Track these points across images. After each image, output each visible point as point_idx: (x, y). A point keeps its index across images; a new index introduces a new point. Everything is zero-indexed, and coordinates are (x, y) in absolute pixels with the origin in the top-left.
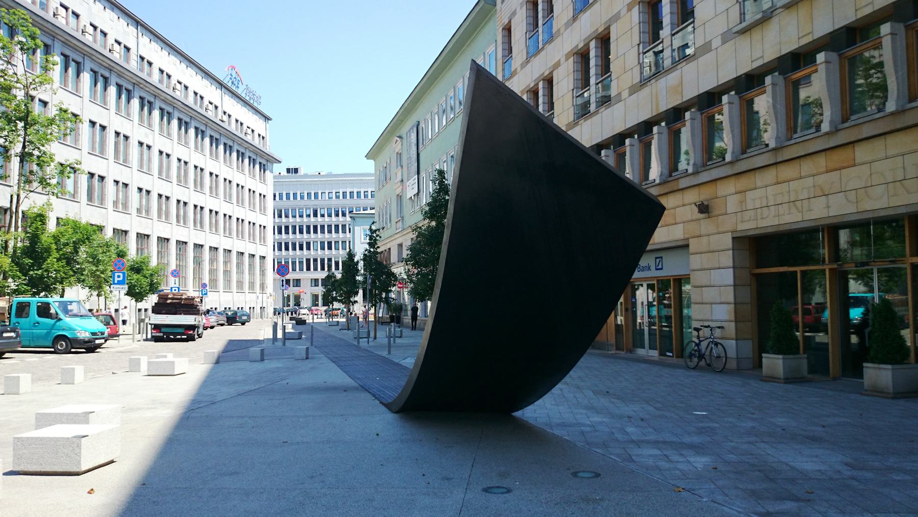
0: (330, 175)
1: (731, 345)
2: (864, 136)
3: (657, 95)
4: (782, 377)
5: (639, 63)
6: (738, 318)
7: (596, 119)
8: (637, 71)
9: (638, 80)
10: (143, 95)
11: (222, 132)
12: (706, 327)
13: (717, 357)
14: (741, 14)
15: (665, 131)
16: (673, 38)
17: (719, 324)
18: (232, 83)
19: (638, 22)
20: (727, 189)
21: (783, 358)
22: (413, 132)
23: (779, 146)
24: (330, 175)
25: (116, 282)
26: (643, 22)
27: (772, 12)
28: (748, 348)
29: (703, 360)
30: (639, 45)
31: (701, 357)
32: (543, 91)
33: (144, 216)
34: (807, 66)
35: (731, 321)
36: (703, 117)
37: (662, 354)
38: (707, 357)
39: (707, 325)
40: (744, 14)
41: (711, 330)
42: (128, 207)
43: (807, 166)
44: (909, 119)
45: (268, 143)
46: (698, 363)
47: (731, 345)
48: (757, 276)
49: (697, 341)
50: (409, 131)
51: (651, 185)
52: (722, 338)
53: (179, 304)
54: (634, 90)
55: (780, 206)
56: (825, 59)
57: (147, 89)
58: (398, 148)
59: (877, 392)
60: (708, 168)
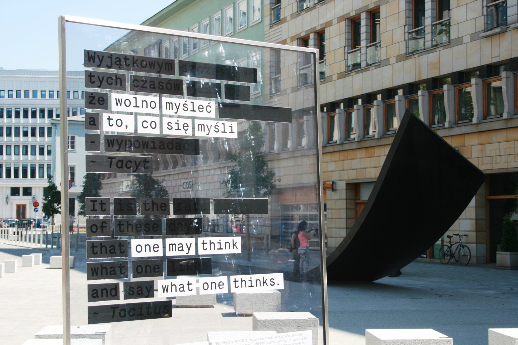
1: (472, 247)
3: (419, 66)
4: (509, 266)
5: (345, 59)
6: (478, 230)
8: (343, 63)
9: (404, 52)
12: (456, 235)
13: (464, 255)
14: (406, 48)
15: (403, 99)
16: (367, 49)
17: (464, 233)
19: (404, 9)
21: (510, 254)
23: (509, 118)
26: (348, 32)
27: (506, 28)
28: (483, 249)
29: (454, 258)
30: (405, 26)
31: (452, 255)
34: (467, 82)
35: (473, 231)
36: (456, 89)
38: (456, 256)
39: (457, 234)
40: (408, 47)
41: (460, 237)
44: (514, 123)
46: (450, 260)
47: (472, 247)
48: (491, 201)
49: (449, 245)
51: (351, 141)
52: (466, 243)
55: (508, 156)
56: (422, 94)
60: (459, 125)
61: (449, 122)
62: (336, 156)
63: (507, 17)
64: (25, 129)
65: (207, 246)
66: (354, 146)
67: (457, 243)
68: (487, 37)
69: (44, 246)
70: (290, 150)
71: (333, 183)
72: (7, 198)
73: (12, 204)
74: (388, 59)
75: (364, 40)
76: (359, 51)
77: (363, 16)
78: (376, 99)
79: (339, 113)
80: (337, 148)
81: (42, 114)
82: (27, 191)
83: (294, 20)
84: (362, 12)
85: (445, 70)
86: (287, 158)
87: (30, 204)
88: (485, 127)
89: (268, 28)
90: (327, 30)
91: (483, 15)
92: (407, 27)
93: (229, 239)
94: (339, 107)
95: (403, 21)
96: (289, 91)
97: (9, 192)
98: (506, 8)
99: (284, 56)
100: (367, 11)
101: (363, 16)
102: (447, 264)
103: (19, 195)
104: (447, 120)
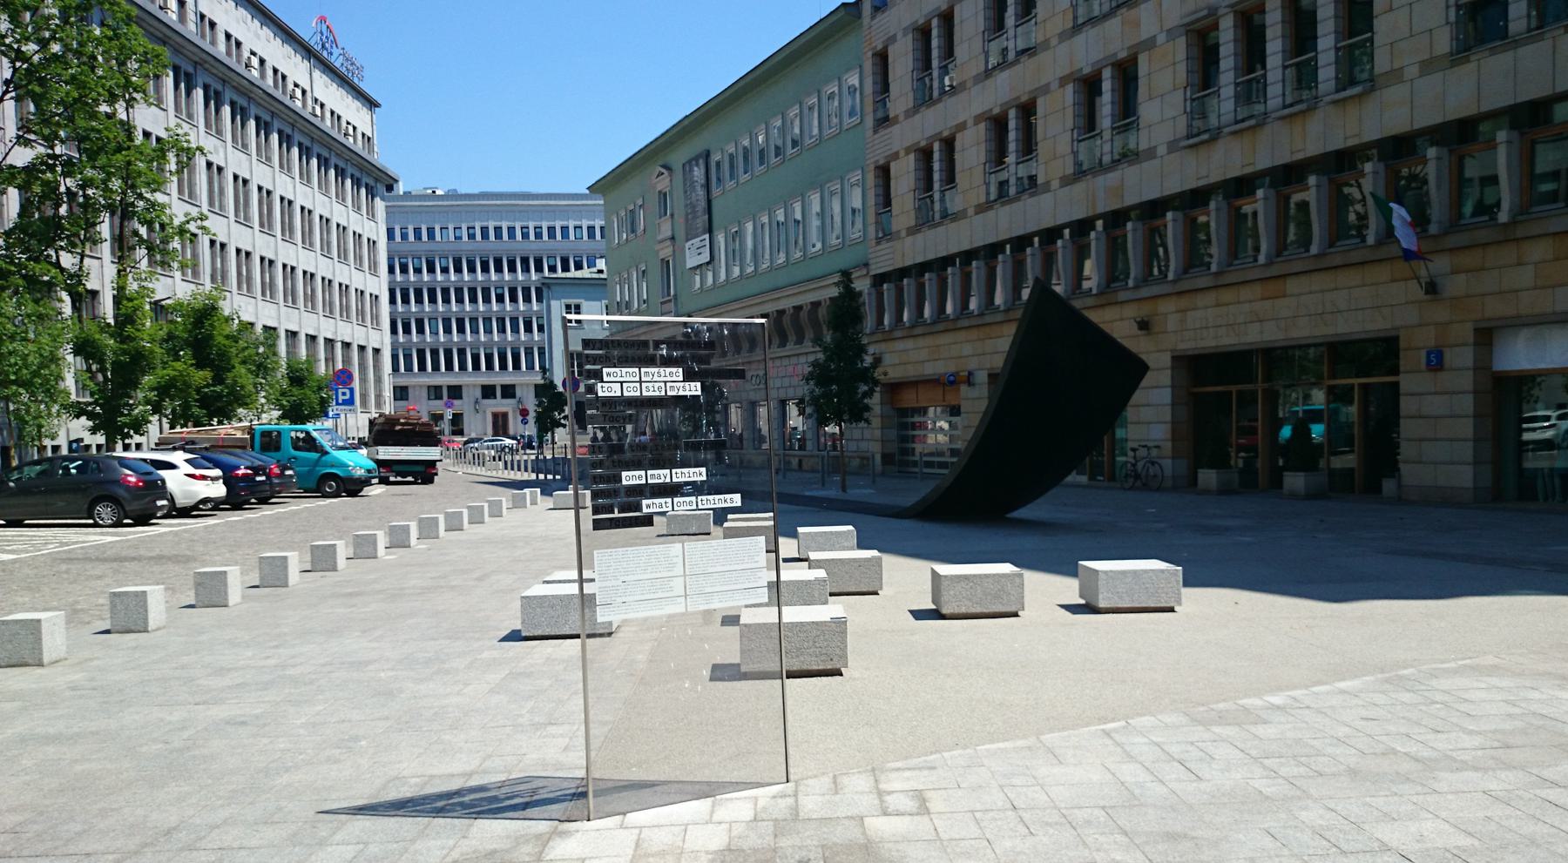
0: (452, 195)
1: (1167, 464)
2: (1295, 270)
7: (1016, 206)
8: (1070, 161)
10: (209, 80)
11: (315, 136)
12: (1144, 446)
15: (1103, 238)
17: (1156, 444)
18: (323, 46)
20: (1167, 307)
22: (697, 165)
24: (453, 196)
25: (340, 401)
30: (1073, 130)
31: (1137, 476)
32: (940, 155)
33: (245, 293)
37: (1092, 478)
42: (199, 273)
43: (1246, 293)
45: (376, 149)
47: (1167, 464)
49: (1133, 461)
50: (690, 162)
52: (1159, 458)
53: (412, 431)
54: (1067, 181)
57: (215, 71)
58: (663, 184)
59: (1294, 496)
61: (1135, 278)
62: (974, 334)
63: (1506, 20)
64: (499, 291)
65: (679, 475)
66: (999, 317)
67: (1144, 458)
68: (1191, 146)
69: (533, 476)
70: (907, 325)
71: (970, 374)
72: (476, 402)
73: (485, 412)
74: (965, 210)
75: (1106, 116)
76: (1099, 138)
77: (1012, 114)
78: (1093, 228)
79: (1004, 262)
80: (974, 322)
81: (524, 266)
82: (508, 392)
83: (910, 120)
84: (1105, 66)
85: (1131, 199)
86: (903, 338)
87: (514, 411)
88: (1185, 285)
89: (870, 132)
90: (959, 136)
91: (1185, 112)
92: (1075, 131)
93: (697, 470)
94: (1004, 252)
95: (1070, 123)
96: (903, 233)
97: (478, 393)
98: (1265, 85)
99: (1174, 64)
100: (1113, 65)
101: (1012, 114)
102: (1131, 488)
103: (495, 398)
104: (1132, 275)
